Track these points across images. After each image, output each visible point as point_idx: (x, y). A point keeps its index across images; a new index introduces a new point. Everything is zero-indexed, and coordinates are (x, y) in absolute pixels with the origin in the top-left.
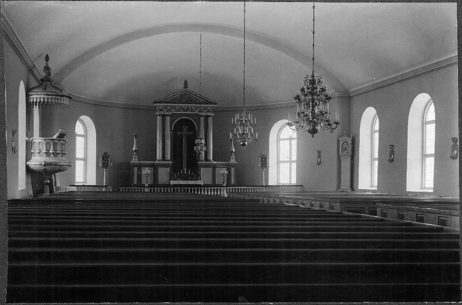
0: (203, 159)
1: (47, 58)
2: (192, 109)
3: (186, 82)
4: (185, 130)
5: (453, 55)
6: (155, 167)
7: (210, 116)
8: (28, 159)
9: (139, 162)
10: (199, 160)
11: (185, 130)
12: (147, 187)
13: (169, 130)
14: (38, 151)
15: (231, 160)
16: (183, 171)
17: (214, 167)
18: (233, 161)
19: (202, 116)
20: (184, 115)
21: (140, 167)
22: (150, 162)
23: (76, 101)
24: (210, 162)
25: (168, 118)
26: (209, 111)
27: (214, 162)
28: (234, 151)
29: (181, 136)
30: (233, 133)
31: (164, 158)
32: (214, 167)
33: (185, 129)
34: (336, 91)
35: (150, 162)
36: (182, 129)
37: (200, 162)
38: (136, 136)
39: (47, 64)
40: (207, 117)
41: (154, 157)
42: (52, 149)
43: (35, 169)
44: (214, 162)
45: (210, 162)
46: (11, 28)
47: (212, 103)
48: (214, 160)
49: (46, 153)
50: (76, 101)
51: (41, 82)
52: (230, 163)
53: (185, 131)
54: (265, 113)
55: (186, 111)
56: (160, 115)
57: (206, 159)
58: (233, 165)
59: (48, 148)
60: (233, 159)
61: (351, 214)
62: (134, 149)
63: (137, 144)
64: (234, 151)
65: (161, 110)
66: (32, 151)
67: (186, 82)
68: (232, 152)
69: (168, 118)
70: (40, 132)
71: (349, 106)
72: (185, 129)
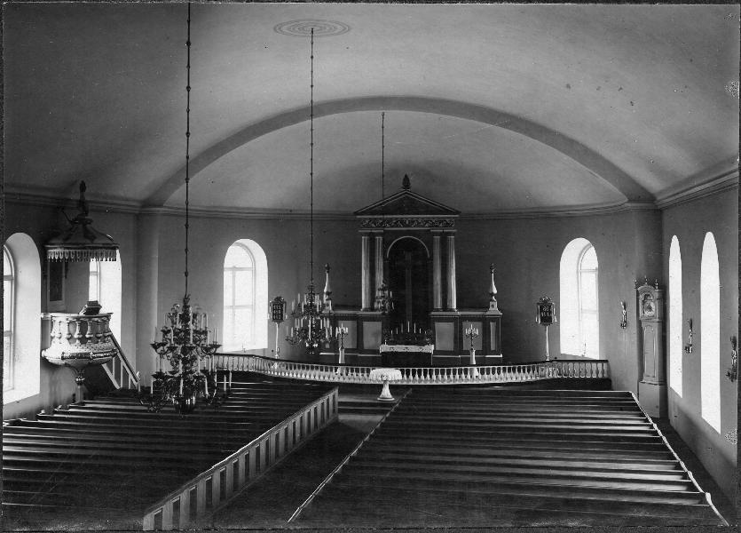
0: (455, 307)
1: (83, 187)
3: (406, 178)
5: (732, 169)
6: (358, 321)
7: (449, 234)
8: (45, 342)
10: (433, 309)
12: (341, 365)
13: (381, 260)
14: (59, 336)
15: (491, 309)
16: (405, 328)
18: (494, 309)
19: (437, 234)
20: (408, 232)
24: (452, 313)
25: (379, 239)
26: (447, 225)
27: (459, 313)
28: (495, 291)
32: (459, 323)
33: (408, 256)
34: (630, 201)
37: (433, 313)
38: (328, 268)
39: (82, 196)
40: (444, 236)
42: (78, 332)
43: (53, 362)
44: (459, 313)
45: (452, 313)
47: (451, 213)
48: (459, 307)
49: (68, 339)
52: (488, 313)
54: (554, 227)
56: (366, 234)
57: (445, 307)
58: (494, 318)
59: (71, 330)
60: (493, 306)
61: (78, 424)
62: (325, 291)
63: (330, 284)
64: (495, 291)
65: (368, 226)
66: (52, 335)
67: (406, 178)
68: (492, 294)
69: (379, 239)
70: (361, 96)
71: (661, 219)
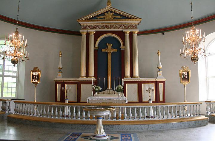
2: (116, 26)
4: (109, 47)
9: (62, 79)
11: (109, 47)
17: (140, 84)
21: (63, 84)
22: (75, 79)
23: (22, 108)
29: (106, 53)
30: (182, 50)
31: (87, 75)
33: (110, 46)
35: (75, 79)
36: (107, 46)
41: (79, 76)
46: (88, 133)
48: (140, 76)
50: (22, 108)
51: (133, 117)
53: (110, 49)
55: (110, 28)
72: (110, 46)
